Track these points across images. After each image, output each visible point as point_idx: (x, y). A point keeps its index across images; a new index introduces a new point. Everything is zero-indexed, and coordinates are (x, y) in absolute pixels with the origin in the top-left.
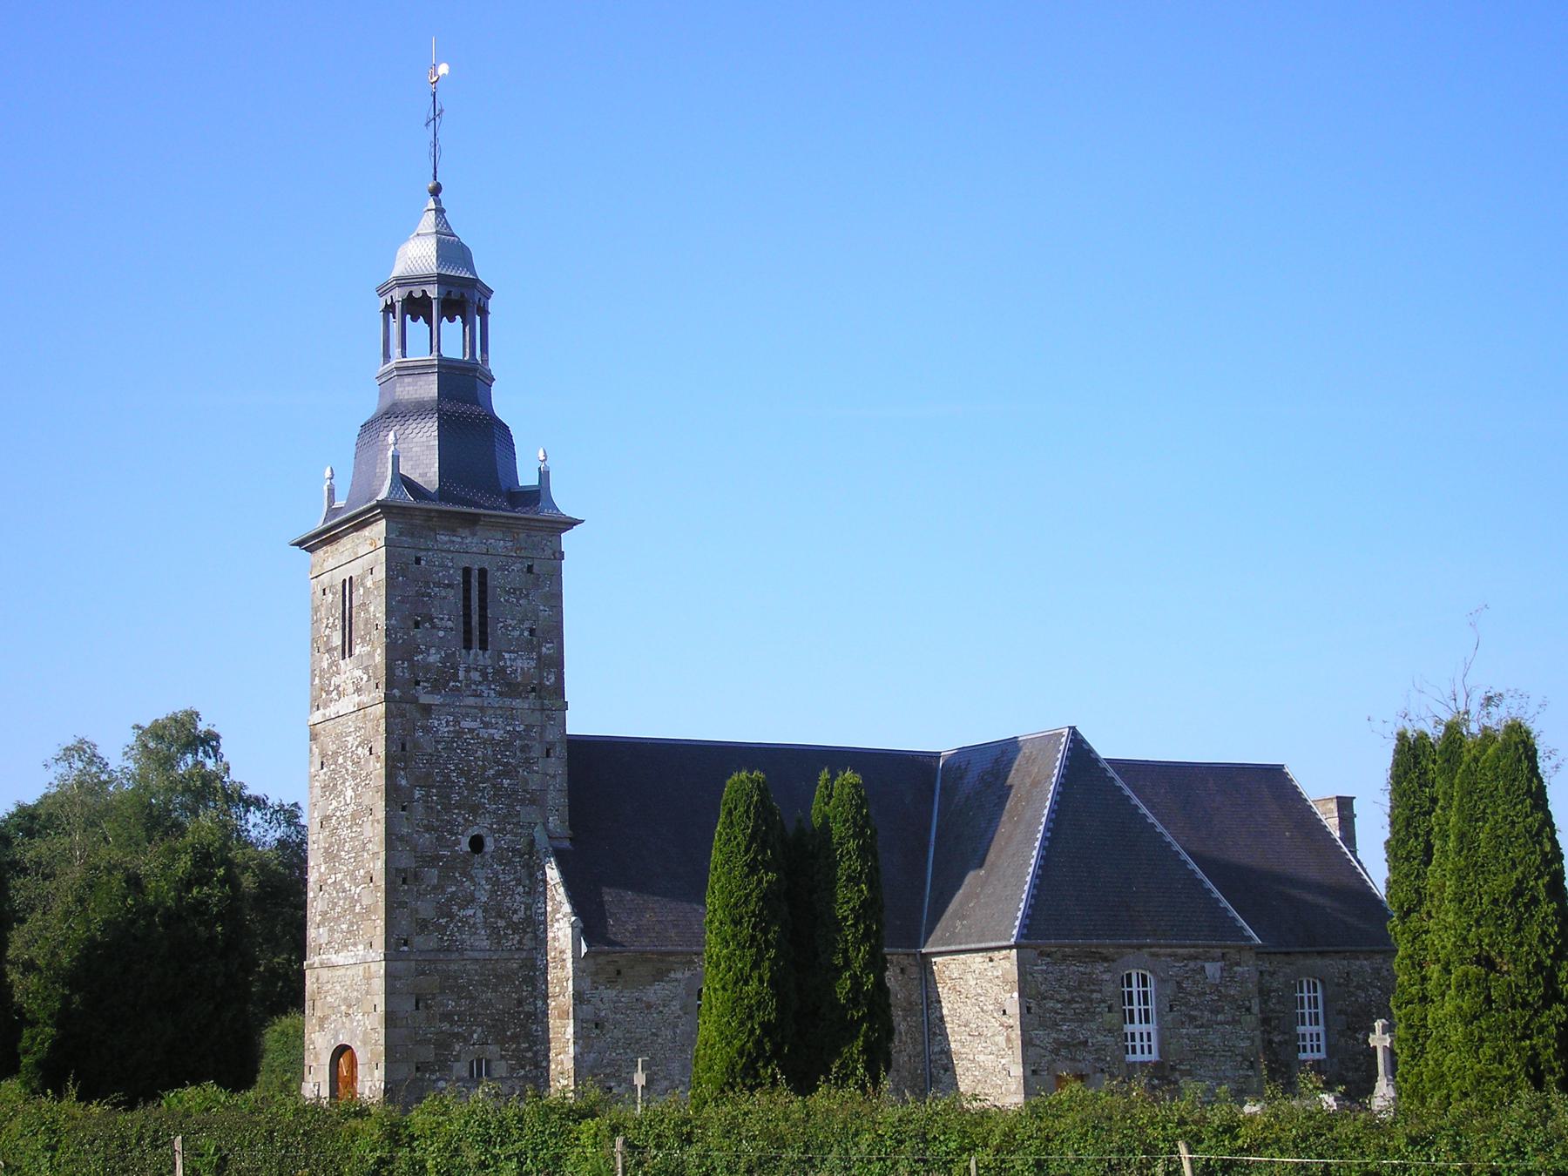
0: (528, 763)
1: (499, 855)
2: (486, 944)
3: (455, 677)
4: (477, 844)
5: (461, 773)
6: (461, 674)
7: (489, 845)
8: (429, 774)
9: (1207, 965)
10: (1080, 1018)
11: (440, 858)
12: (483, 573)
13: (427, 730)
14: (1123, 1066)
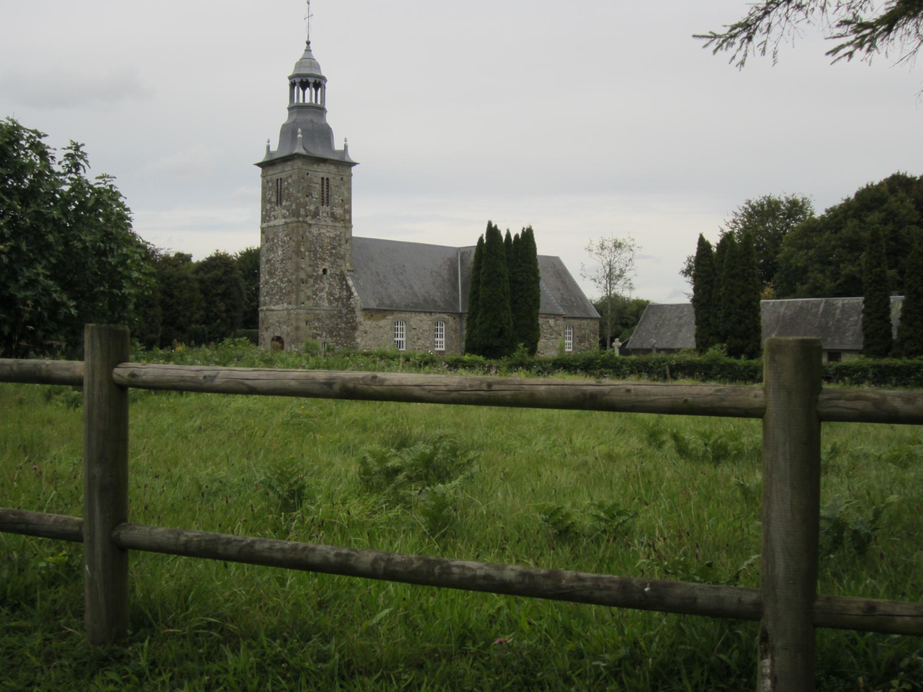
1: (331, 276)
2: (327, 305)
3: (318, 215)
4: (325, 271)
7: (329, 272)
12: (328, 179)
13: (310, 232)
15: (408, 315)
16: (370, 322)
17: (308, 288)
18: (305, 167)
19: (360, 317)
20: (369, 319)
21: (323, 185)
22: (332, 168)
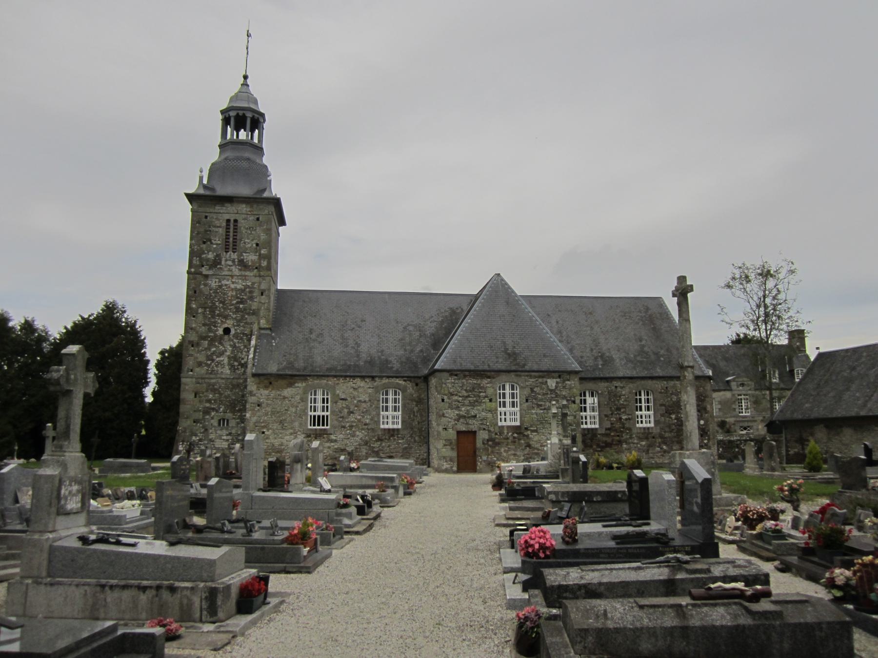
0: (251, 298)
1: (236, 336)
2: (228, 372)
3: (220, 263)
4: (227, 331)
5: (221, 302)
6: (223, 263)
7: (233, 332)
8: (206, 303)
9: (549, 381)
10: (472, 404)
11: (209, 337)
12: (236, 221)
13: (206, 285)
14: (497, 428)
15: (331, 382)
16: (267, 392)
17: (199, 352)
18: (201, 209)
19: (252, 386)
20: (266, 387)
21: (228, 232)
22: (243, 208)
